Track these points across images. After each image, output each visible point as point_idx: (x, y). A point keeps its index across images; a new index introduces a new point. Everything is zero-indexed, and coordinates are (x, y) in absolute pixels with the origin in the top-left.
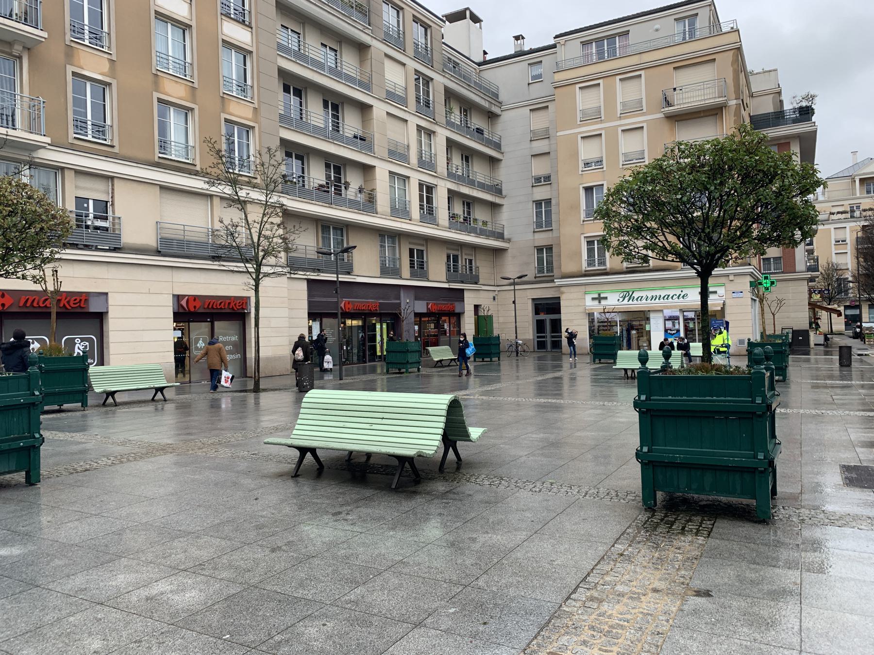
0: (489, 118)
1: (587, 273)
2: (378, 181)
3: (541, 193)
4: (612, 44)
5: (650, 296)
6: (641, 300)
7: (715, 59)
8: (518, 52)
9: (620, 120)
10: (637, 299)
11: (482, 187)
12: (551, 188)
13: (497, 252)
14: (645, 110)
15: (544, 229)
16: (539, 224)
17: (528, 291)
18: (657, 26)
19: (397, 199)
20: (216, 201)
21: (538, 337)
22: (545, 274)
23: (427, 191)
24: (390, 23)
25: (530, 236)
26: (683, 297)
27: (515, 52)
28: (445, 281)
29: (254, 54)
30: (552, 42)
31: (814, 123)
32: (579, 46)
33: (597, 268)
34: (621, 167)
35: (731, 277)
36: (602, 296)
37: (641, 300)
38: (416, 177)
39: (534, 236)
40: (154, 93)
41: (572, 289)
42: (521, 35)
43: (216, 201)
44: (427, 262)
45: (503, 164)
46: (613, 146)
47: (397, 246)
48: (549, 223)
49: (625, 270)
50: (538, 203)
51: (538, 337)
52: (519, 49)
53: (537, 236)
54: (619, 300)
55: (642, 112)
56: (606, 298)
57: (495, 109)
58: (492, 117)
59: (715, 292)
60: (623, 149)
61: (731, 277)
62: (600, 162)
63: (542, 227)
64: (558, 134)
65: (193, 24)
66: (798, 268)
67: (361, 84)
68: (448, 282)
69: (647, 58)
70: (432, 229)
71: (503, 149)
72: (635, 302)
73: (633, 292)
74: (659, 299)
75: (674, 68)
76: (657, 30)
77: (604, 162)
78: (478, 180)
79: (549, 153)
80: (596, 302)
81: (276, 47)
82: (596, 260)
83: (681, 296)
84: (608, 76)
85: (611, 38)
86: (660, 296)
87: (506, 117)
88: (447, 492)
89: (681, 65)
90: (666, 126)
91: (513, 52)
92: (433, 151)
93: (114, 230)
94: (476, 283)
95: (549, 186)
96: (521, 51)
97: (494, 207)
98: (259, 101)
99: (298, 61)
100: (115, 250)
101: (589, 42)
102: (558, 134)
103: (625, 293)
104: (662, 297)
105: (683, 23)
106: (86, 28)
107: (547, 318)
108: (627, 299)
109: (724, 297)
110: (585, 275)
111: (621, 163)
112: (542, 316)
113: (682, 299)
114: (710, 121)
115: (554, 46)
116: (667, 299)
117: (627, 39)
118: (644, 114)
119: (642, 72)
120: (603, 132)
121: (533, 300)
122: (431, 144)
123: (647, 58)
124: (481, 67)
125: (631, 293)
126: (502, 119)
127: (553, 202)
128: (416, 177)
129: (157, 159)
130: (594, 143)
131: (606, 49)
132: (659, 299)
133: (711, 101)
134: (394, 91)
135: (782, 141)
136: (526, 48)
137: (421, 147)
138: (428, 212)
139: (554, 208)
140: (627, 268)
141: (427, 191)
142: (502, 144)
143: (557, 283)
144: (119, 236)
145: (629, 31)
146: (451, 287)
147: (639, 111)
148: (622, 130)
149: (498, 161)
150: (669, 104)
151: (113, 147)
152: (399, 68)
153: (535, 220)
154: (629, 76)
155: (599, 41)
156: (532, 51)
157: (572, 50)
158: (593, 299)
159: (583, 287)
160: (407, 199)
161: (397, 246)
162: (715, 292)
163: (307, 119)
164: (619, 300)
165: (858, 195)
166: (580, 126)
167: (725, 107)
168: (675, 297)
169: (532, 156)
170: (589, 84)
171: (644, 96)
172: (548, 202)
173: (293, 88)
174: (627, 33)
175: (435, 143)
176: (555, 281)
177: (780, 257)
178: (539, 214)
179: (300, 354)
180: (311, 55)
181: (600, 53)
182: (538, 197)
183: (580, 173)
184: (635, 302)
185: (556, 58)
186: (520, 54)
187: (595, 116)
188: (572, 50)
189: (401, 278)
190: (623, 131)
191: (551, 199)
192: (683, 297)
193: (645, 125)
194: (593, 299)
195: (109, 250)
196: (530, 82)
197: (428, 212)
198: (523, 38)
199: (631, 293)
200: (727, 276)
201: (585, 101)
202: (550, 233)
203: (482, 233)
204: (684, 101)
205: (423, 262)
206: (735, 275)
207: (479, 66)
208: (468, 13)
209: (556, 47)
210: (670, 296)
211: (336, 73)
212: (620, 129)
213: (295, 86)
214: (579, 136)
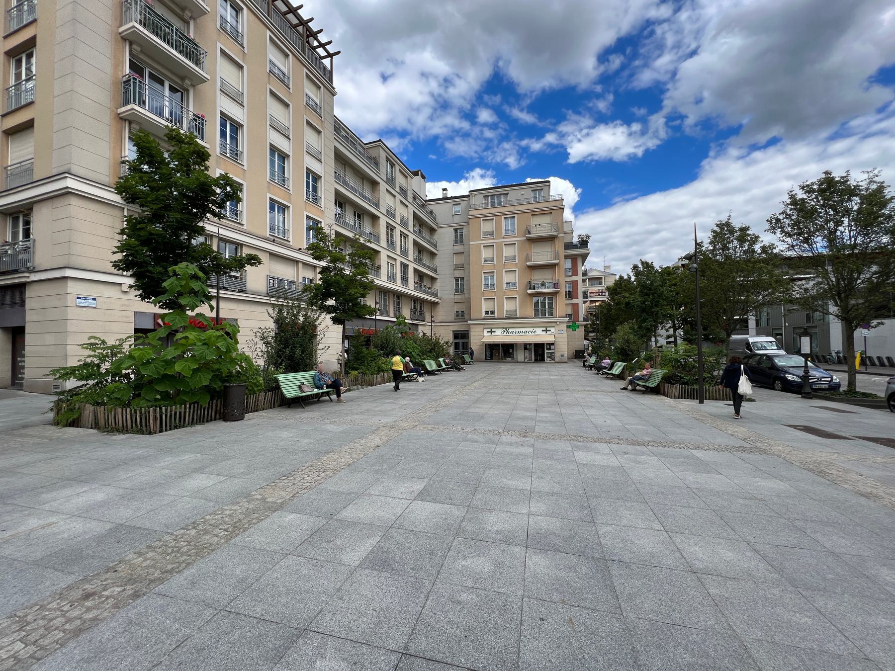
3: (458, 274)
5: (517, 331)
11: (428, 268)
13: (434, 305)
18: (523, 193)
20: (300, 265)
23: (404, 267)
29: (323, 178)
30: (468, 194)
35: (558, 323)
36: (493, 330)
38: (399, 259)
40: (268, 194)
41: (478, 326)
43: (300, 265)
44: (401, 308)
50: (457, 279)
53: (456, 296)
58: (432, 230)
61: (558, 323)
62: (492, 260)
64: (471, 243)
65: (290, 154)
66: (580, 320)
67: (375, 204)
69: (518, 208)
76: (523, 194)
77: (495, 260)
80: (489, 334)
84: (499, 215)
87: (439, 231)
88: (71, 480)
89: (536, 214)
90: (527, 244)
91: (441, 197)
93: (241, 278)
94: (424, 321)
100: (242, 291)
102: (471, 243)
105: (106, 180)
106: (228, 146)
107: (460, 341)
110: (484, 319)
112: (457, 341)
114: (549, 244)
118: (516, 237)
119: (516, 215)
120: (495, 244)
123: (518, 208)
127: (465, 279)
128: (399, 259)
129: (268, 236)
138: (404, 279)
139: (465, 282)
141: (404, 267)
144: (245, 283)
150: (529, 233)
151: (243, 225)
152: (392, 198)
154: (509, 217)
155: (493, 196)
157: (478, 200)
158: (488, 332)
170: (488, 219)
171: (494, 230)
178: (457, 285)
179: (511, 351)
181: (493, 204)
182: (457, 276)
186: (445, 198)
188: (478, 200)
189: (389, 316)
194: (488, 332)
195: (239, 291)
197: (404, 279)
200: (556, 322)
201: (485, 227)
202: (463, 295)
203: (428, 293)
206: (560, 322)
208: (420, 172)
214: (503, 243)
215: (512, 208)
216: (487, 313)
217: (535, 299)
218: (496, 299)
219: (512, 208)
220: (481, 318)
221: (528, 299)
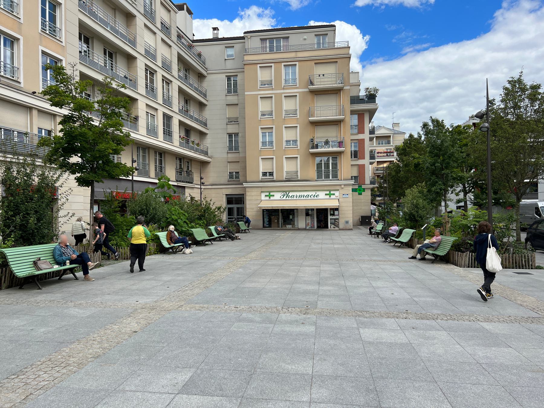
0: (199, 77)
1: (262, 180)
2: (139, 110)
3: (232, 129)
4: (271, 42)
5: (298, 195)
6: (293, 197)
7: (337, 62)
8: (215, 38)
9: (284, 90)
10: (291, 197)
11: (197, 120)
12: (239, 126)
13: (204, 164)
14: (298, 86)
15: (234, 151)
16: (230, 148)
17: (213, 190)
18: (305, 37)
19: (149, 123)
20: (35, 112)
21: (229, 218)
22: (234, 179)
23: (167, 119)
24: (147, 2)
25: (225, 155)
26: (317, 196)
27: (213, 38)
28: (175, 181)
29: (63, 6)
30: (242, 35)
31: (377, 104)
32: (259, 41)
33: (268, 177)
34: (283, 118)
35: (343, 186)
37: (293, 197)
38: (161, 110)
39: (228, 155)
41: (254, 190)
42: (217, 28)
43: (35, 112)
45: (207, 108)
46: (279, 105)
47: (147, 155)
48: (237, 148)
49: (284, 179)
50: (230, 135)
51: (229, 218)
52: (215, 36)
53: (230, 155)
54: (281, 197)
55: (296, 86)
56: (274, 196)
57: (204, 73)
58: (201, 77)
59: (334, 194)
60: (285, 108)
63: (233, 150)
64: (246, 93)
67: (130, 41)
68: (177, 181)
69: (300, 55)
70: (170, 146)
71: (208, 98)
72: (290, 198)
73: (289, 193)
74: (303, 197)
75: (315, 63)
76: (305, 39)
78: (195, 116)
79: (238, 104)
81: (78, 5)
82: (323, 171)
83: (315, 196)
84: (278, 62)
85: (278, 39)
86: (304, 195)
87: (209, 78)
89: (320, 62)
90: (310, 97)
92: (170, 94)
94: (192, 183)
95: (237, 125)
96: (217, 38)
97: (202, 135)
98: (66, 42)
99: (91, 17)
101: (265, 39)
103: (284, 193)
104: (290, 196)
107: (235, 206)
108: (285, 196)
109: (338, 197)
110: (261, 182)
111: (283, 116)
113: (316, 198)
115: (242, 38)
116: (308, 197)
117: (288, 41)
120: (273, 96)
121: (226, 195)
122: (169, 89)
123: (300, 55)
124: (193, 44)
125: (288, 193)
126: (207, 79)
127: (240, 135)
128: (161, 110)
130: (267, 103)
131: (275, 46)
132: (303, 197)
133: (329, 86)
134: (149, 50)
135: (360, 113)
136: (220, 36)
137: (164, 90)
138: (168, 133)
139: (240, 139)
140: (285, 178)
141: (167, 119)
142: (207, 95)
143: (244, 186)
145: (289, 37)
146: (179, 185)
147: (294, 87)
148: (260, 97)
149: (205, 105)
150: (312, 83)
153: (228, 146)
154: (290, 65)
156: (224, 39)
157: (254, 43)
159: (260, 188)
160: (156, 123)
161: (147, 155)
162: (334, 194)
163: (93, 58)
164: (281, 197)
165: (375, 145)
166: (260, 90)
167: (342, 90)
168: (312, 196)
169: (227, 105)
170: (266, 66)
172: (237, 134)
173: (84, 36)
174: (288, 38)
175: (172, 89)
176: (243, 184)
177: (357, 176)
178: (231, 141)
180: (99, 15)
182: (230, 131)
183: (259, 119)
184: (290, 198)
185: (244, 46)
186: (216, 39)
187: (268, 84)
189: (149, 177)
190: (285, 96)
191: (238, 133)
192: (317, 196)
193: (298, 94)
194: (266, 196)
196: (226, 58)
197: (168, 133)
198: (218, 30)
199: (288, 193)
200: (340, 185)
201: (263, 75)
203: (196, 151)
204: (319, 84)
205: (162, 167)
206: (345, 185)
207: (193, 43)
208: (185, 7)
209: (245, 39)
210: (309, 196)
211: (115, 31)
212: (283, 95)
213: (85, 35)
214: (259, 96)
215: (293, 55)
216: (264, 174)
217: (318, 159)
218: (274, 159)
219: (293, 55)
220: (257, 180)
221: (310, 159)
